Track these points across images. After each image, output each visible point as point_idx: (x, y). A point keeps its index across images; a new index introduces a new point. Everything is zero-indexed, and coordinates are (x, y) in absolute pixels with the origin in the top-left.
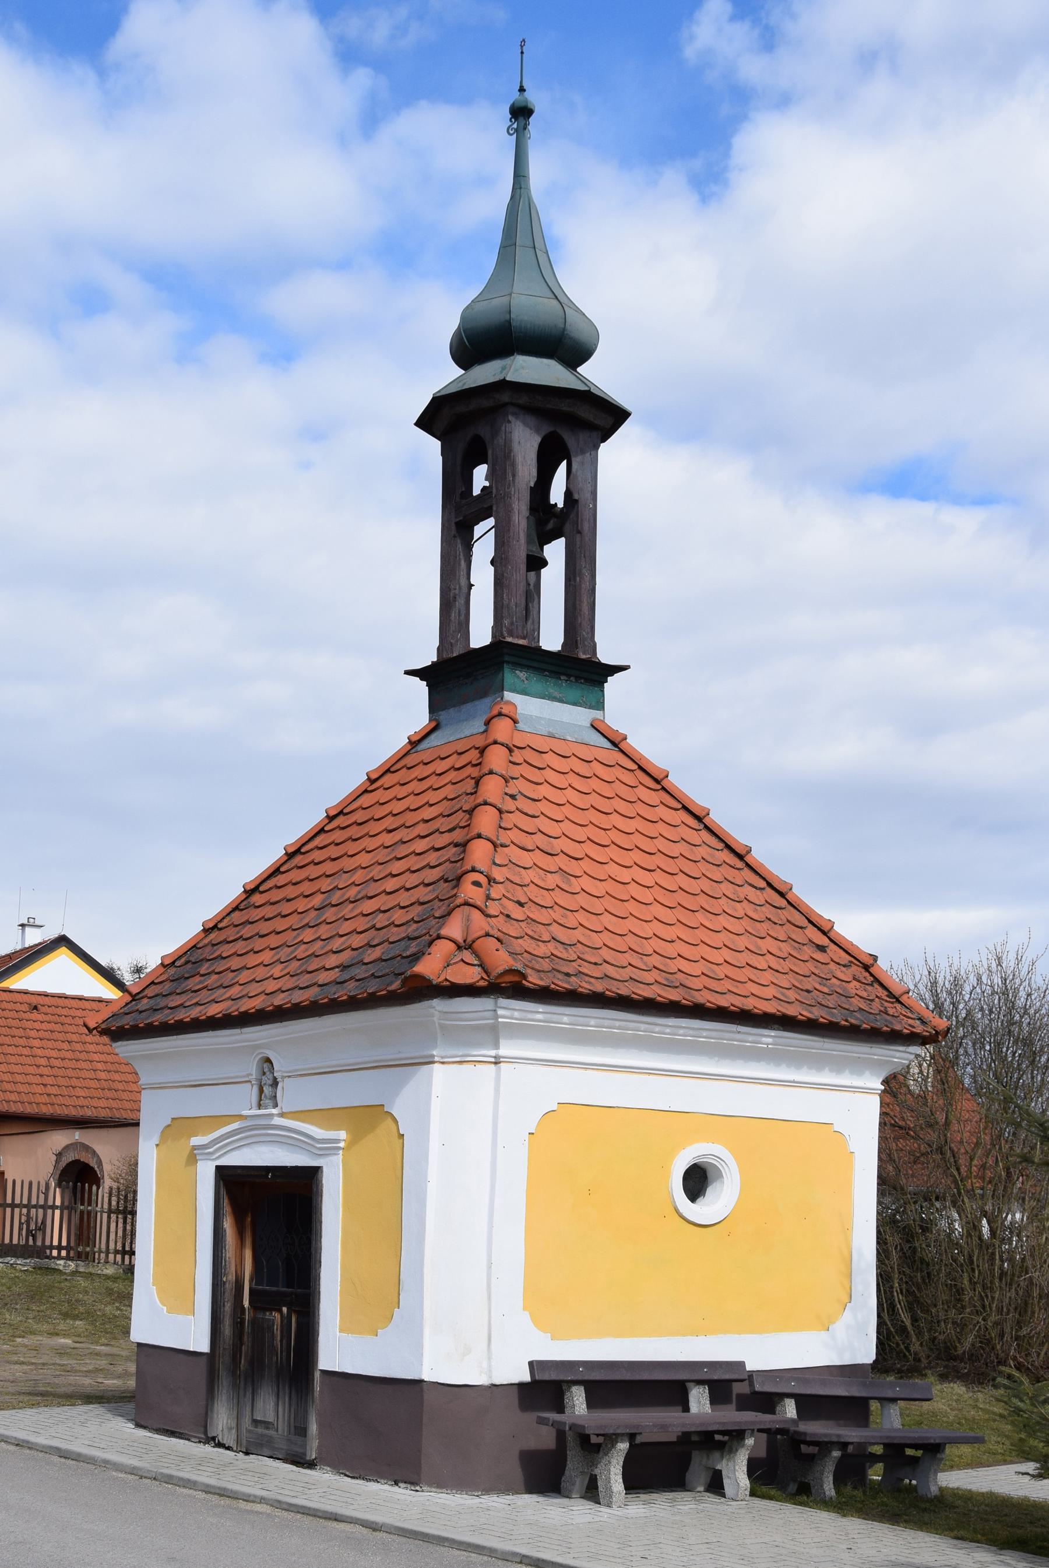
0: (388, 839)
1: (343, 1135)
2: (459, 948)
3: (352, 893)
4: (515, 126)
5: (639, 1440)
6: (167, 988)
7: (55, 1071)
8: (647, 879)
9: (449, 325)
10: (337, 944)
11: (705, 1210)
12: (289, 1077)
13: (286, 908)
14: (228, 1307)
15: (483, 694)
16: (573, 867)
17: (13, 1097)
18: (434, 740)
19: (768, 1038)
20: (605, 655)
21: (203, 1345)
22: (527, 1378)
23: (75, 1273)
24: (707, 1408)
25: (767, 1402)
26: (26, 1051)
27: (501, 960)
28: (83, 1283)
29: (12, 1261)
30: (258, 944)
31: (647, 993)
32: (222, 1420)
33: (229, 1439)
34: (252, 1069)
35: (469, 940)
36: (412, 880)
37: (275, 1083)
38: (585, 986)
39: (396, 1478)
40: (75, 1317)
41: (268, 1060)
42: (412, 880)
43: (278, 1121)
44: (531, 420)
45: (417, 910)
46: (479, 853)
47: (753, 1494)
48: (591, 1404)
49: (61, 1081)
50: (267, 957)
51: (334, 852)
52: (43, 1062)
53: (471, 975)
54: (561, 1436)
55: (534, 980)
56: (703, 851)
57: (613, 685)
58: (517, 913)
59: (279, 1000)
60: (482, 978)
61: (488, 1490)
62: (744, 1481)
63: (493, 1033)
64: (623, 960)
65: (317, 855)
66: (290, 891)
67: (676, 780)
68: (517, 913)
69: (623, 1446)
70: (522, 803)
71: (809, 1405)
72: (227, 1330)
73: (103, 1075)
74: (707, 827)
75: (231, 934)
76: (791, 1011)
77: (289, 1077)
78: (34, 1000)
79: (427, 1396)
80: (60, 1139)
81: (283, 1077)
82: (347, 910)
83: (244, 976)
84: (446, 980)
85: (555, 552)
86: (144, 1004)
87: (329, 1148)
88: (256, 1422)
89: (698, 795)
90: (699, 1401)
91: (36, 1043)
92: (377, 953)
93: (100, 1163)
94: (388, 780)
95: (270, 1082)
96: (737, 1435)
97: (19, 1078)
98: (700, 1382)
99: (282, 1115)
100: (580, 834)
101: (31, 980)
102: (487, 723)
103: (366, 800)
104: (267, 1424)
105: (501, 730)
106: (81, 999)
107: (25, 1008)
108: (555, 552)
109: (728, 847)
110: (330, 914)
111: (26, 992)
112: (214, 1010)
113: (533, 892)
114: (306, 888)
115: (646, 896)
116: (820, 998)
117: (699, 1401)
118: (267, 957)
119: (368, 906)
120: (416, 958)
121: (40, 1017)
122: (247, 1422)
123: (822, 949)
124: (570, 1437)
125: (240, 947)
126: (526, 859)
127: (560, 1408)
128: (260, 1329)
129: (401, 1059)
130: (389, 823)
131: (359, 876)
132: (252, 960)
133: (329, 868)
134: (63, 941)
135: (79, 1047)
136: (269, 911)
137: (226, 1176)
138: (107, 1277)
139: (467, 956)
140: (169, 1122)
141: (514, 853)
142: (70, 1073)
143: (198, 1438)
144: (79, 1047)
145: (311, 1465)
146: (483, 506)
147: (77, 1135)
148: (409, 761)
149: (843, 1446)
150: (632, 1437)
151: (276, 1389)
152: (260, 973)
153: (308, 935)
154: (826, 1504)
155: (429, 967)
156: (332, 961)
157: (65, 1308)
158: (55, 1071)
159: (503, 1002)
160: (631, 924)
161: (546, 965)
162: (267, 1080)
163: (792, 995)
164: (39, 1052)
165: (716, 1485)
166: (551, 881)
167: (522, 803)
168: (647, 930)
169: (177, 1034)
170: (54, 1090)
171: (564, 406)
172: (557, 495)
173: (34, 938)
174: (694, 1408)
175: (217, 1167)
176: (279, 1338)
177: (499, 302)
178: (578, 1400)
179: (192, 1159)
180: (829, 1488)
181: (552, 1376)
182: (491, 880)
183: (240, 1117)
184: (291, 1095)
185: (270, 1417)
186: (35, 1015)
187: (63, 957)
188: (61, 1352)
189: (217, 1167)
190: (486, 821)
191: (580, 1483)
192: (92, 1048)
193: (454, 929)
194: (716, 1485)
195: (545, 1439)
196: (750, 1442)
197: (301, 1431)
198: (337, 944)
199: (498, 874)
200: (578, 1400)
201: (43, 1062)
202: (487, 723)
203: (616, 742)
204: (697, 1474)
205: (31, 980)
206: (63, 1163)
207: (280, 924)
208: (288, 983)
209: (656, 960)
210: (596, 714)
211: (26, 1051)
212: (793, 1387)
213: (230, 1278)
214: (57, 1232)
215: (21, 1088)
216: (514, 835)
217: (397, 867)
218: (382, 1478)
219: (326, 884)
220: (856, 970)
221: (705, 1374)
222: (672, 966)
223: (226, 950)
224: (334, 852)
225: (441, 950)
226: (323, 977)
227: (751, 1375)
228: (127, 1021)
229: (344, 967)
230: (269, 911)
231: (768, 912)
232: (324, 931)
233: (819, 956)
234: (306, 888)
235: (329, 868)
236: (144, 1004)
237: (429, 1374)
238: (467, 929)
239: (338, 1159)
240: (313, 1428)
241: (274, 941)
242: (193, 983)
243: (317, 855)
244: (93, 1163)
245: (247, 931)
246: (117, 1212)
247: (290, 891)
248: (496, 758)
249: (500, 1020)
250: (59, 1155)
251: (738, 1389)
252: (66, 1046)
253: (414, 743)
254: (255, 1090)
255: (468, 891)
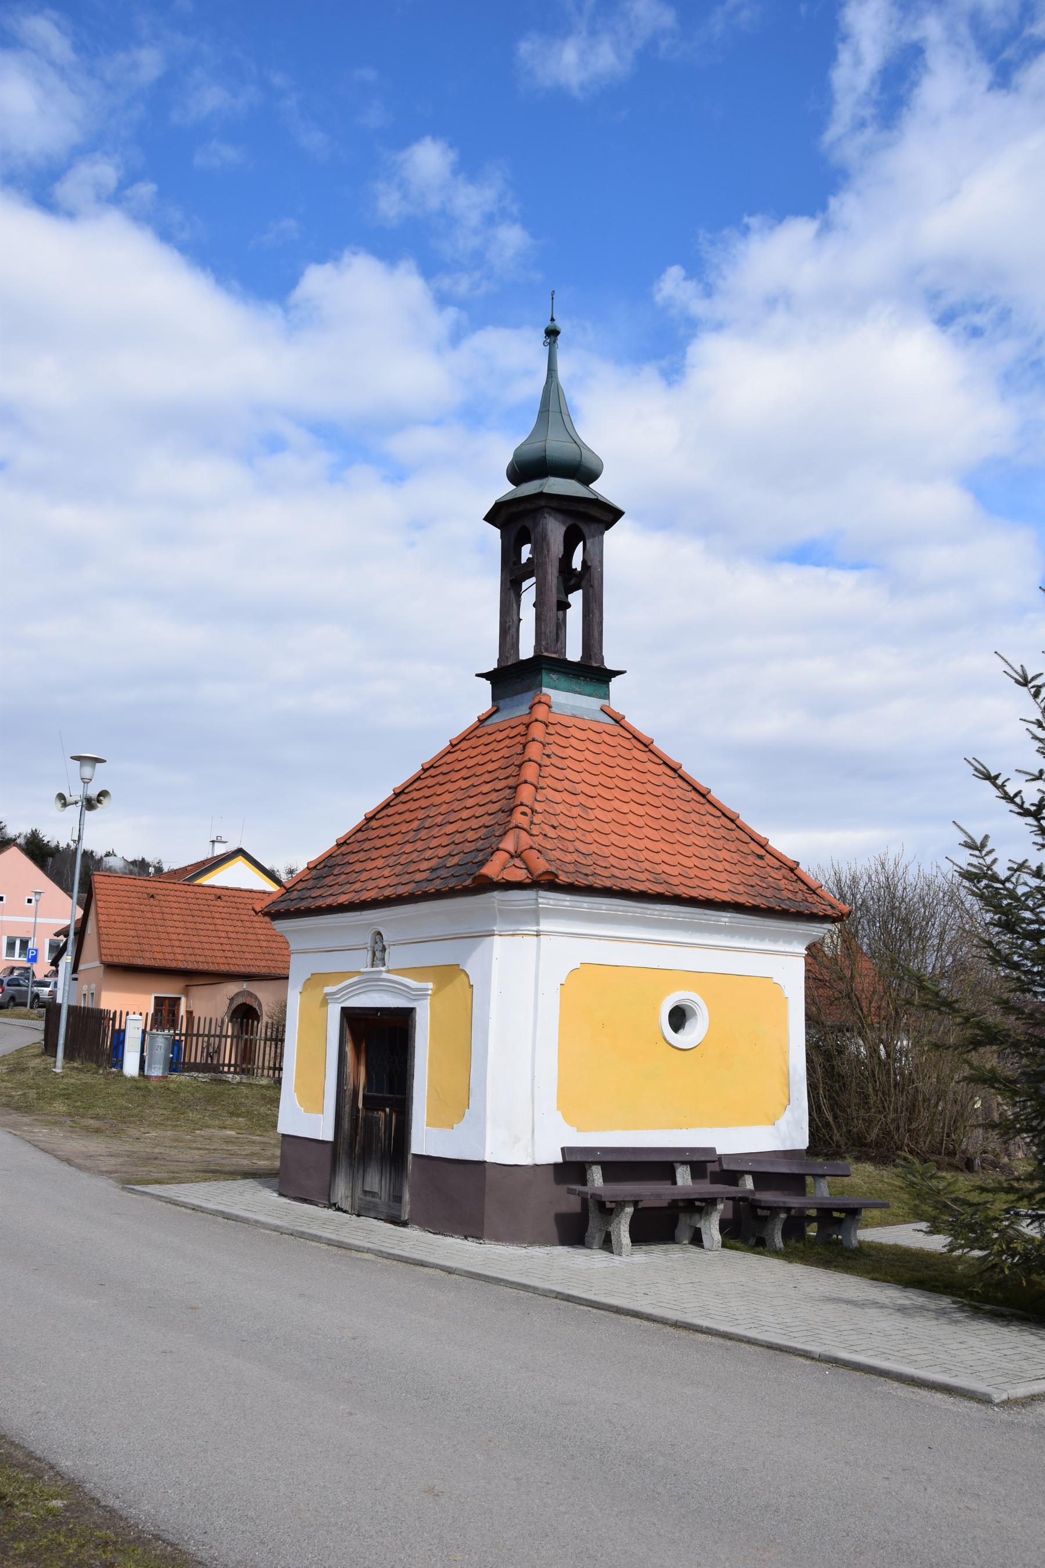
0: (464, 784)
1: (430, 985)
2: (512, 856)
3: (439, 819)
4: (548, 341)
5: (641, 1205)
6: (310, 884)
7: (231, 941)
8: (640, 810)
9: (506, 458)
10: (428, 854)
11: (686, 1038)
12: (394, 945)
13: (393, 830)
14: (347, 1108)
15: (528, 689)
16: (590, 803)
17: (201, 959)
18: (496, 719)
19: (725, 918)
20: (610, 664)
21: (328, 1135)
22: (560, 1160)
23: (240, 1083)
24: (689, 1182)
25: (732, 1177)
26: (212, 927)
27: (541, 865)
28: (245, 1090)
29: (195, 1074)
30: (374, 854)
31: (641, 887)
32: (341, 1191)
33: (346, 1206)
34: (368, 940)
35: (519, 851)
36: (480, 811)
37: (384, 949)
38: (599, 883)
39: (466, 1234)
40: (239, 1115)
41: (379, 934)
42: (480, 811)
43: (385, 976)
44: (560, 517)
45: (483, 831)
46: (526, 793)
47: (724, 1246)
48: (606, 1179)
49: (235, 948)
50: (380, 863)
51: (427, 792)
52: (223, 934)
53: (520, 875)
54: (584, 1202)
55: (563, 878)
56: (678, 792)
57: (615, 683)
58: (551, 833)
59: (387, 892)
60: (528, 877)
61: (532, 1243)
62: (717, 1236)
63: (536, 915)
64: (625, 864)
65: (415, 795)
66: (397, 819)
67: (659, 745)
68: (551, 833)
69: (629, 1210)
70: (554, 760)
71: (763, 1179)
72: (346, 1124)
73: (264, 944)
74: (680, 776)
75: (355, 847)
76: (741, 899)
77: (394, 945)
78: (218, 892)
79: (489, 1173)
80: (232, 988)
81: (390, 945)
82: (435, 831)
83: (364, 876)
84: (503, 878)
85: (576, 598)
86: (295, 895)
87: (421, 994)
88: (365, 1192)
89: (674, 755)
90: (683, 1176)
91: (219, 922)
92: (455, 860)
93: (260, 1005)
94: (464, 745)
95: (380, 949)
96: (711, 1202)
97: (206, 946)
98: (683, 1163)
99: (388, 971)
100: (594, 780)
101: (217, 878)
102: (531, 708)
103: (449, 758)
104: (373, 1194)
105: (540, 712)
106: (251, 891)
107: (212, 897)
108: (576, 598)
109: (695, 789)
110: (423, 834)
111: (213, 887)
112: (342, 899)
113: (562, 819)
114: (408, 816)
115: (640, 822)
116: (761, 890)
117: (683, 1176)
118: (380, 863)
119: (450, 829)
120: (482, 863)
121: (222, 904)
122: (359, 1193)
123: (761, 857)
124: (591, 1204)
125: (362, 856)
126: (557, 797)
127: (584, 1182)
128: (370, 1124)
129: (472, 933)
130: (465, 773)
131: (443, 809)
132: (370, 865)
133: (424, 803)
134: (240, 852)
135: (248, 924)
136: (382, 832)
137: (346, 1012)
138: (262, 1087)
139: (517, 862)
140: (309, 977)
141: (549, 793)
142: (241, 942)
143: (324, 1204)
144: (248, 924)
145: (404, 1224)
146: (528, 570)
147: (245, 986)
148: (478, 732)
149: (788, 1210)
150: (635, 1203)
151: (380, 1167)
152: (375, 874)
153: (408, 848)
154: (777, 1254)
155: (492, 869)
156: (425, 865)
157: (232, 1108)
158: (231, 941)
159: (542, 893)
160: (630, 840)
161: (571, 868)
162: (379, 947)
163: (741, 889)
164: (221, 928)
165: (697, 1240)
166: (575, 812)
167: (554, 760)
168: (641, 845)
169: (317, 916)
170: (230, 954)
171: (581, 508)
172: (577, 563)
173: (220, 850)
174: (680, 1181)
175: (342, 1008)
176: (383, 1131)
177: (538, 445)
178: (596, 1175)
179: (325, 1002)
180: (779, 1242)
181: (579, 1158)
182: (533, 811)
183: (359, 973)
184: (395, 957)
185: (376, 1188)
186: (219, 903)
187: (240, 862)
188: (228, 1141)
189: (342, 1008)
190: (530, 772)
191: (599, 1237)
192: (257, 925)
193: (508, 844)
194: (697, 1240)
195: (573, 1205)
196: (721, 1207)
197: (398, 1199)
198: (428, 854)
199: (538, 807)
200: (596, 1175)
201: (223, 934)
202: (531, 708)
203: (618, 720)
204: (683, 1231)
205: (217, 878)
206: (234, 1006)
207: (389, 841)
208: (394, 880)
209: (647, 865)
210: (605, 702)
211: (212, 927)
212: (750, 1166)
213: (350, 1087)
214: (228, 1054)
215: (207, 953)
216: (549, 781)
217: (470, 802)
218: (456, 1234)
219: (421, 814)
220: (785, 872)
221: (687, 1157)
222: (658, 869)
223: (352, 858)
224: (427, 792)
225: (500, 858)
226: (418, 877)
227: (720, 1157)
228: (282, 907)
229: (433, 870)
230: (382, 832)
231: (723, 832)
232: (419, 845)
233: (759, 862)
234: (408, 816)
235: (424, 803)
236: (295, 895)
237: (489, 1158)
238: (517, 843)
239: (427, 1002)
240: (407, 1197)
241: (385, 852)
242: (328, 881)
243: (415, 795)
244: (255, 1006)
245: (367, 845)
246: (271, 1040)
247: (397, 819)
248: (537, 730)
249: (540, 906)
250: (232, 1000)
251: (711, 1168)
252: (239, 924)
253: (481, 721)
254: (370, 954)
255: (518, 818)
